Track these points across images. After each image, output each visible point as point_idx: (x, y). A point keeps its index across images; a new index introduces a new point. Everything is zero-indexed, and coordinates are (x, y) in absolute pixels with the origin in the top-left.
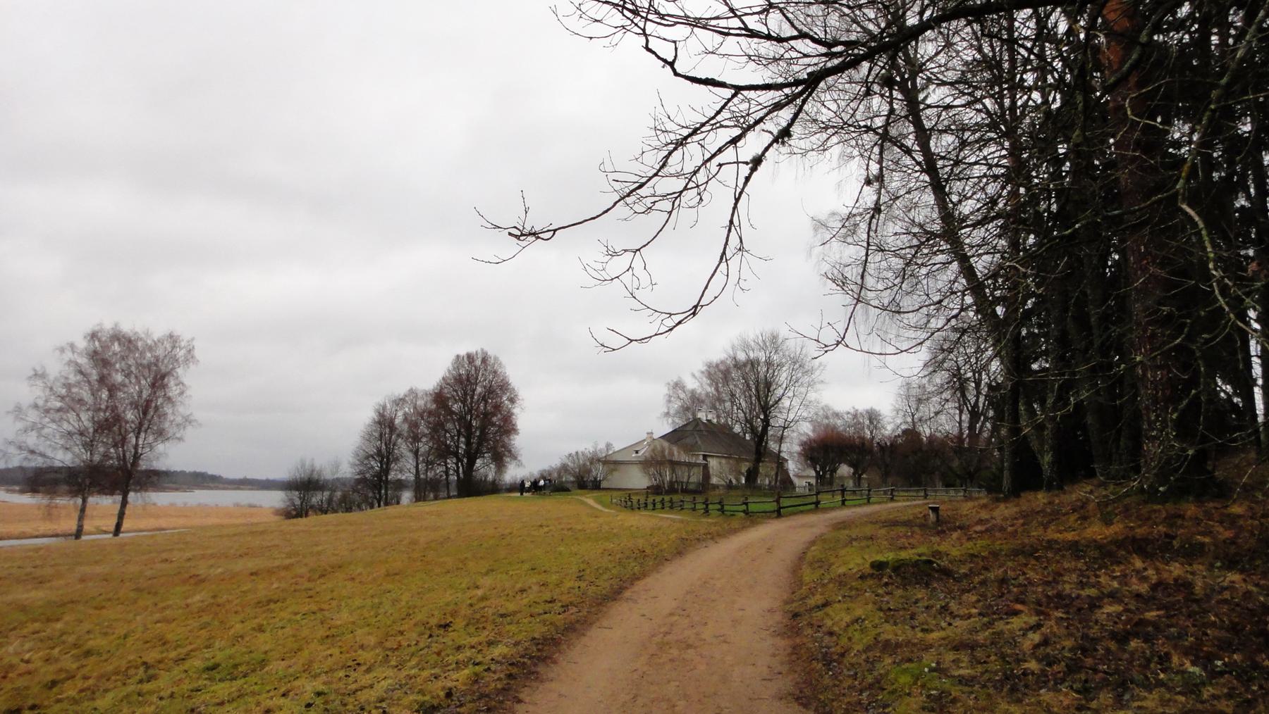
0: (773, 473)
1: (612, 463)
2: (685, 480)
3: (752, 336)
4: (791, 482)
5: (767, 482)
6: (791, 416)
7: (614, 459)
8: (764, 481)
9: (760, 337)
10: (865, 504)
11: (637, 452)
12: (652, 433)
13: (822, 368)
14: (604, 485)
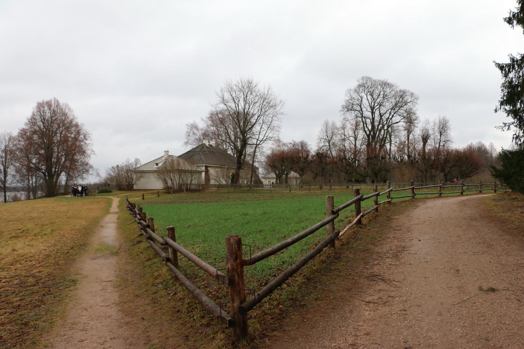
0: (249, 176)
1: (141, 173)
2: (189, 182)
3: (234, 82)
4: (261, 183)
5: (246, 182)
6: (261, 137)
7: (140, 169)
8: (244, 181)
9: (240, 83)
10: (437, 197)
11: (157, 164)
12: (168, 152)
13: (282, 104)
14: (135, 187)
